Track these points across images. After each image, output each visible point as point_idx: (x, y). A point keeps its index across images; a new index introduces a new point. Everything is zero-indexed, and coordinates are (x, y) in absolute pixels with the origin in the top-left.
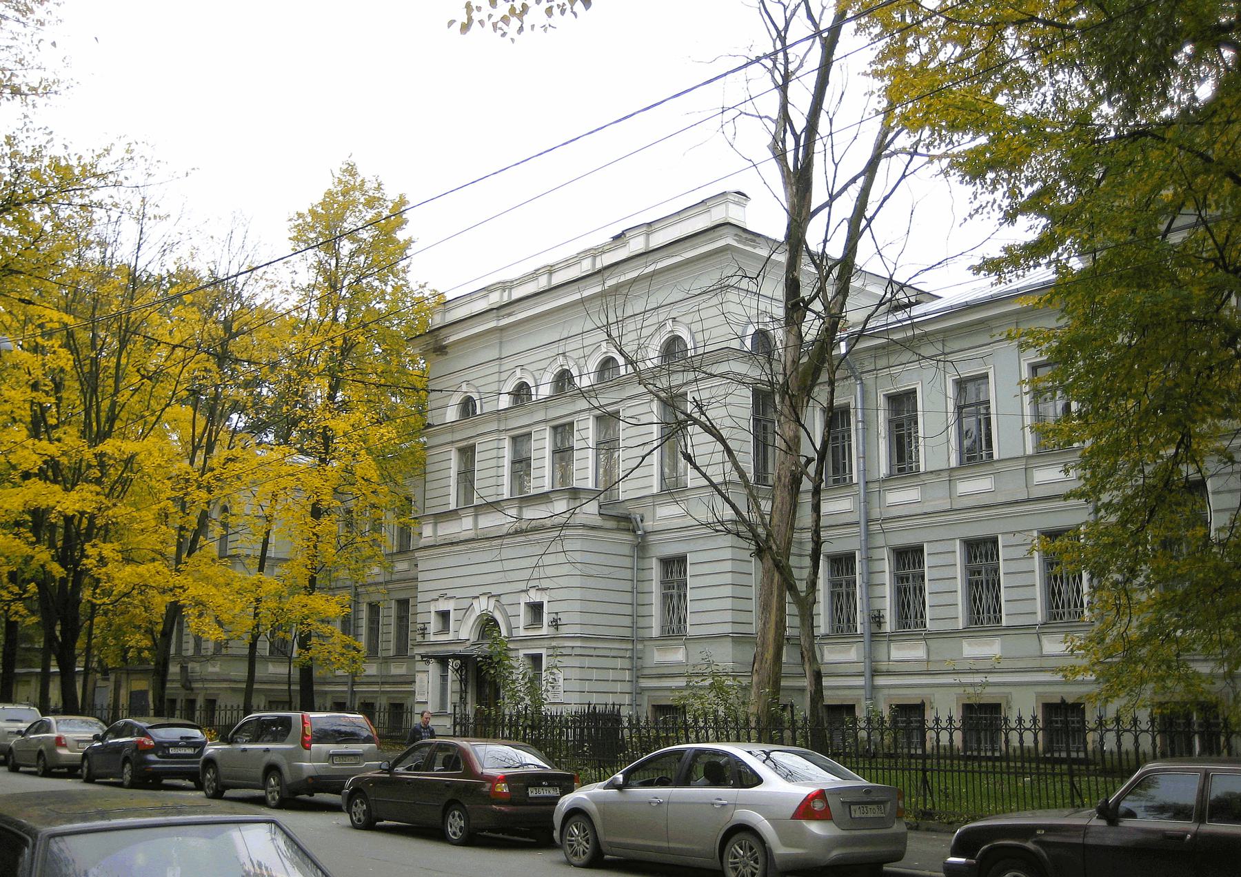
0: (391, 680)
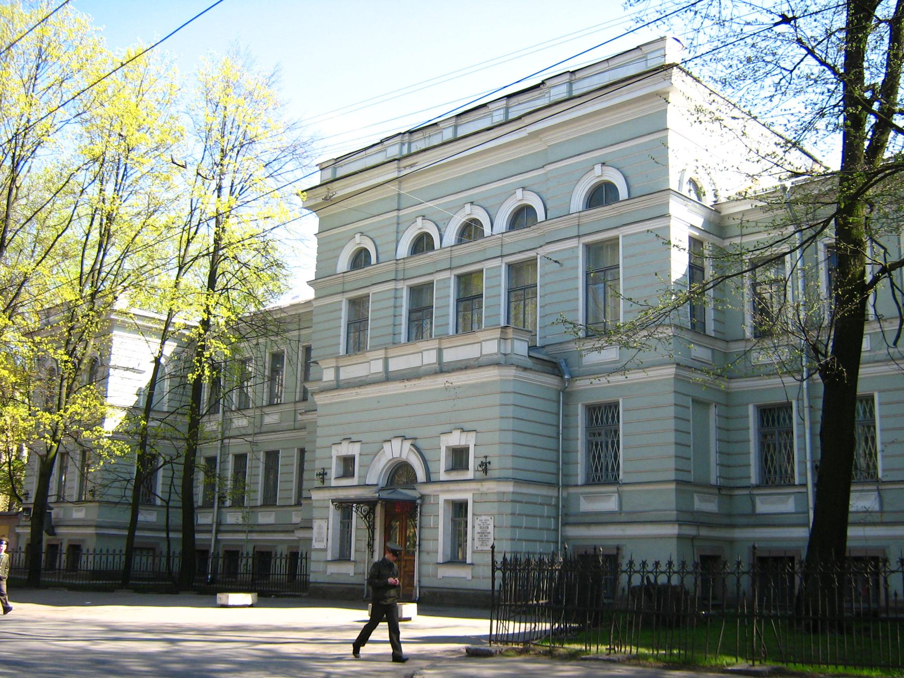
0: (257, 528)
